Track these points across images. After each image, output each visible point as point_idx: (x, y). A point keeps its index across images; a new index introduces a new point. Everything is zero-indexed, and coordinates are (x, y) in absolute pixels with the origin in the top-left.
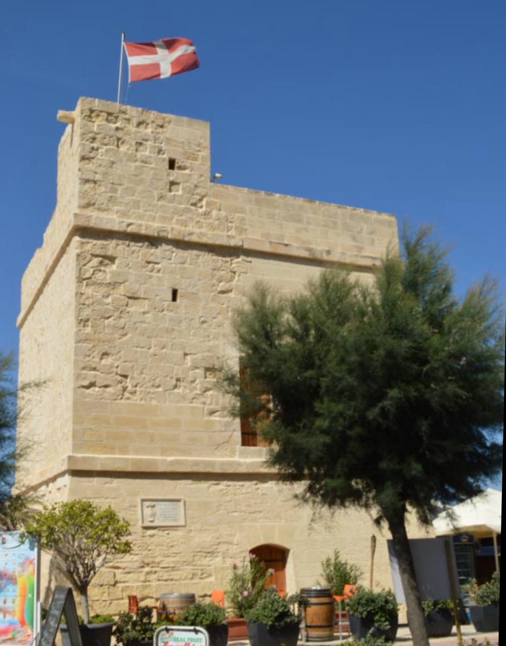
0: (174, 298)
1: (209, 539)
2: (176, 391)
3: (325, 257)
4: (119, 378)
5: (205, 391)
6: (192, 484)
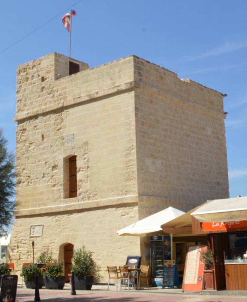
0: (43, 139)
1: (47, 241)
2: (44, 179)
3: (96, 96)
4: (27, 177)
5: (52, 177)
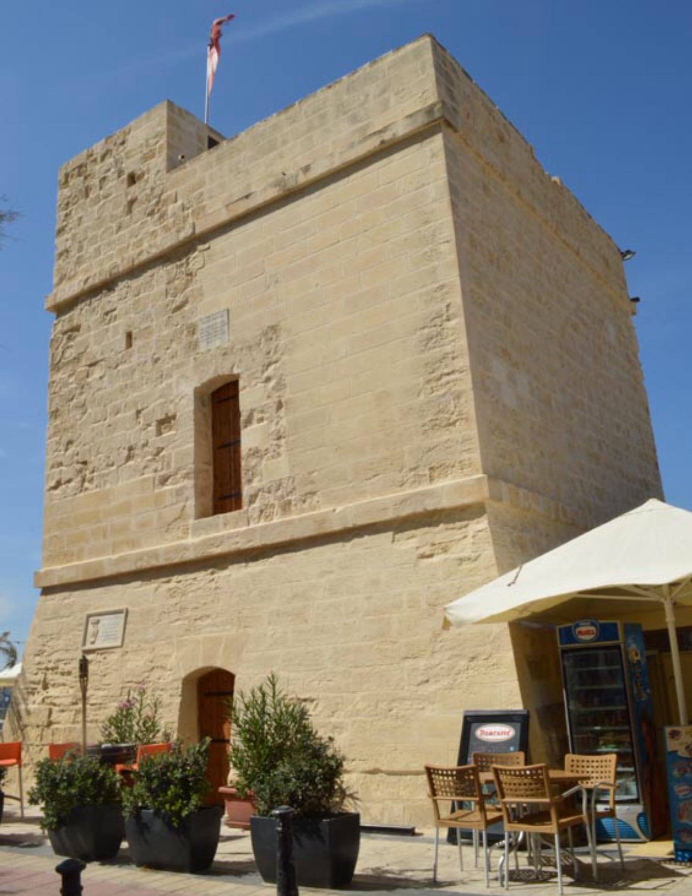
0: (129, 344)
1: (141, 663)
2: (131, 463)
4: (80, 466)
6: (141, 586)
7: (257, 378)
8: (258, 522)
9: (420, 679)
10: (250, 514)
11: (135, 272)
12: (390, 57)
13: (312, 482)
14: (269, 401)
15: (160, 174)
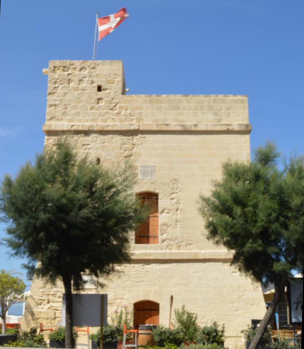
7: (167, 197)
8: (166, 250)
9: (235, 309)
10: (162, 247)
11: (103, 133)
12: (231, 97)
13: (191, 240)
14: (173, 207)
15: (117, 94)
